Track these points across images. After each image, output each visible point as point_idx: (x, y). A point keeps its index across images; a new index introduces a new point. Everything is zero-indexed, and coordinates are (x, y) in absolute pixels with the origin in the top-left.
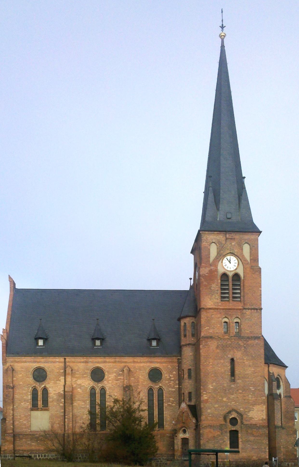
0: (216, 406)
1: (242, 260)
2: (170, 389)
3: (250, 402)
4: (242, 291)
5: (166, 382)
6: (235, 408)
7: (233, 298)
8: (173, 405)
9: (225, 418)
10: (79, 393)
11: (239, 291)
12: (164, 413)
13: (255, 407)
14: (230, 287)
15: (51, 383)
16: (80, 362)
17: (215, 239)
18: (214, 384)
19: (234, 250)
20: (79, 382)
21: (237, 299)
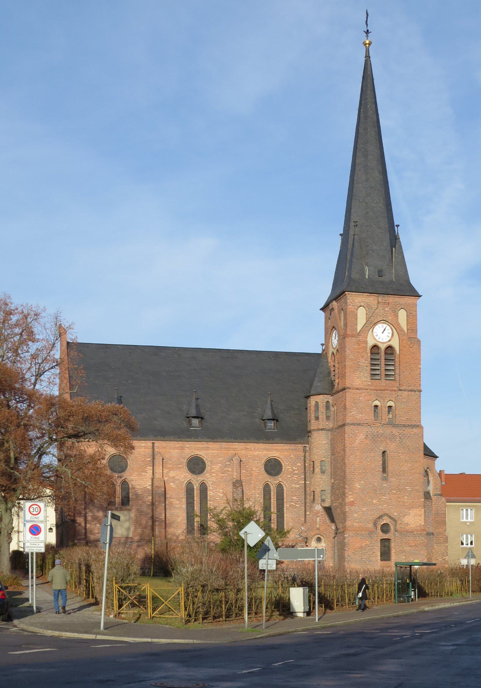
0: (365, 509)
1: (398, 330)
2: (294, 485)
3: (405, 505)
4: (397, 367)
5: (288, 476)
6: (387, 511)
7: (385, 376)
8: (297, 506)
9: (375, 524)
10: (172, 489)
11: (392, 368)
12: (285, 515)
13: (411, 511)
14: (382, 363)
15: (134, 474)
16: (174, 448)
17: (363, 302)
18: (362, 482)
19: (388, 317)
20: (172, 474)
21: (376, 366)
